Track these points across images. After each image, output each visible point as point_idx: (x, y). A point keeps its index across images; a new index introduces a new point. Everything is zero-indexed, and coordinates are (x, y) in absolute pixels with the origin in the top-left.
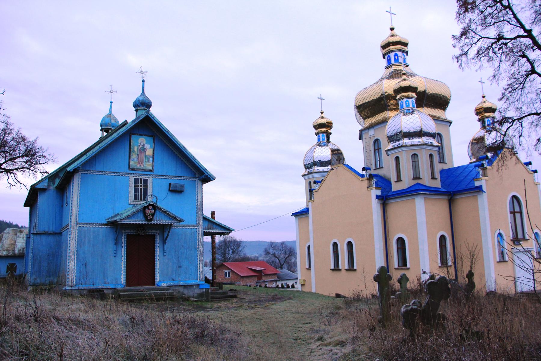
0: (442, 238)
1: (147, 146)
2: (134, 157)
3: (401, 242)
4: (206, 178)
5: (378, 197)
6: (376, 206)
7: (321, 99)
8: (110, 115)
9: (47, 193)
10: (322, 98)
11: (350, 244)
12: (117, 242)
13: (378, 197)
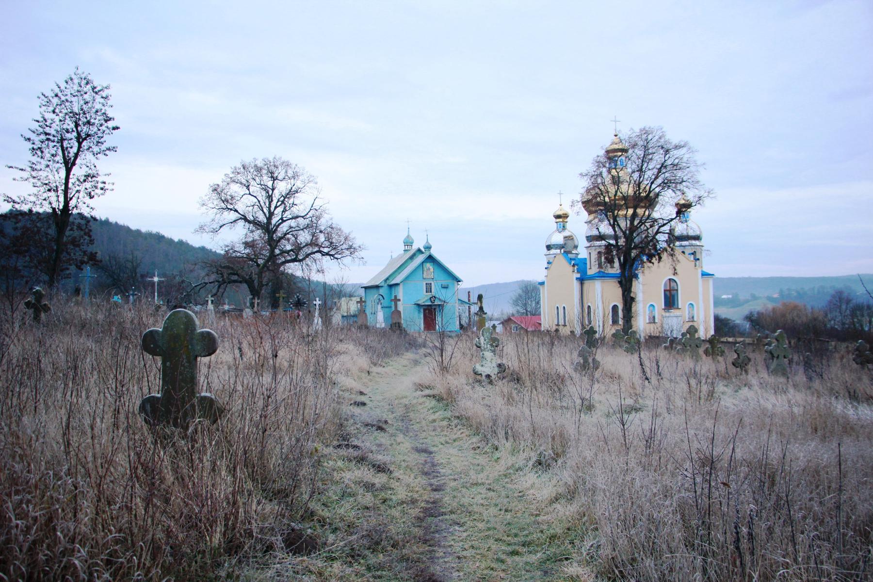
0: (615, 308)
1: (431, 267)
2: (425, 273)
3: (589, 307)
4: (458, 281)
5: (577, 279)
6: (576, 285)
7: (615, 121)
8: (408, 236)
9: (383, 288)
10: (617, 119)
11: (564, 308)
12: (419, 311)
13: (577, 279)
